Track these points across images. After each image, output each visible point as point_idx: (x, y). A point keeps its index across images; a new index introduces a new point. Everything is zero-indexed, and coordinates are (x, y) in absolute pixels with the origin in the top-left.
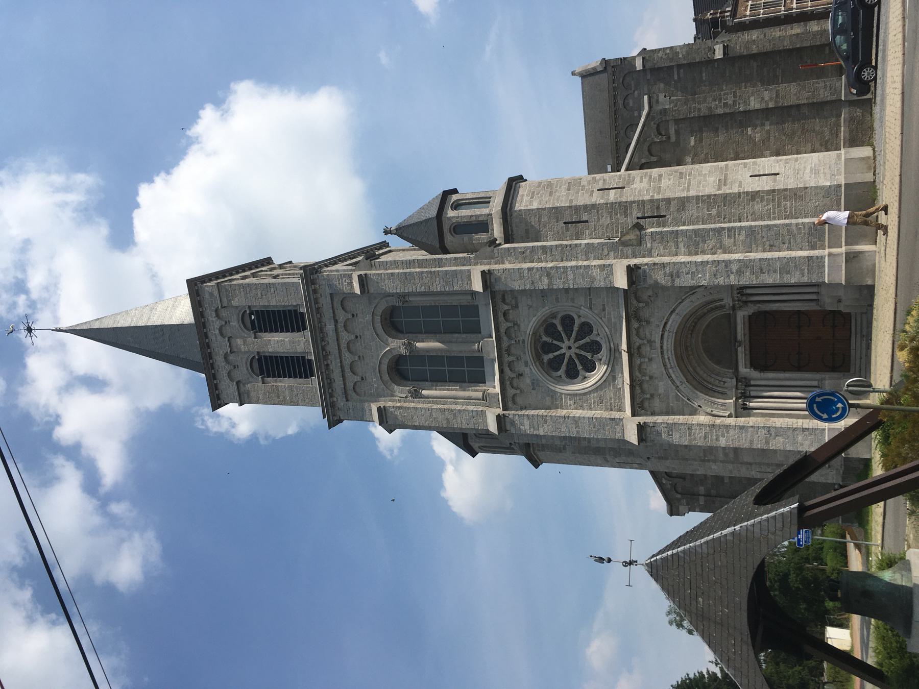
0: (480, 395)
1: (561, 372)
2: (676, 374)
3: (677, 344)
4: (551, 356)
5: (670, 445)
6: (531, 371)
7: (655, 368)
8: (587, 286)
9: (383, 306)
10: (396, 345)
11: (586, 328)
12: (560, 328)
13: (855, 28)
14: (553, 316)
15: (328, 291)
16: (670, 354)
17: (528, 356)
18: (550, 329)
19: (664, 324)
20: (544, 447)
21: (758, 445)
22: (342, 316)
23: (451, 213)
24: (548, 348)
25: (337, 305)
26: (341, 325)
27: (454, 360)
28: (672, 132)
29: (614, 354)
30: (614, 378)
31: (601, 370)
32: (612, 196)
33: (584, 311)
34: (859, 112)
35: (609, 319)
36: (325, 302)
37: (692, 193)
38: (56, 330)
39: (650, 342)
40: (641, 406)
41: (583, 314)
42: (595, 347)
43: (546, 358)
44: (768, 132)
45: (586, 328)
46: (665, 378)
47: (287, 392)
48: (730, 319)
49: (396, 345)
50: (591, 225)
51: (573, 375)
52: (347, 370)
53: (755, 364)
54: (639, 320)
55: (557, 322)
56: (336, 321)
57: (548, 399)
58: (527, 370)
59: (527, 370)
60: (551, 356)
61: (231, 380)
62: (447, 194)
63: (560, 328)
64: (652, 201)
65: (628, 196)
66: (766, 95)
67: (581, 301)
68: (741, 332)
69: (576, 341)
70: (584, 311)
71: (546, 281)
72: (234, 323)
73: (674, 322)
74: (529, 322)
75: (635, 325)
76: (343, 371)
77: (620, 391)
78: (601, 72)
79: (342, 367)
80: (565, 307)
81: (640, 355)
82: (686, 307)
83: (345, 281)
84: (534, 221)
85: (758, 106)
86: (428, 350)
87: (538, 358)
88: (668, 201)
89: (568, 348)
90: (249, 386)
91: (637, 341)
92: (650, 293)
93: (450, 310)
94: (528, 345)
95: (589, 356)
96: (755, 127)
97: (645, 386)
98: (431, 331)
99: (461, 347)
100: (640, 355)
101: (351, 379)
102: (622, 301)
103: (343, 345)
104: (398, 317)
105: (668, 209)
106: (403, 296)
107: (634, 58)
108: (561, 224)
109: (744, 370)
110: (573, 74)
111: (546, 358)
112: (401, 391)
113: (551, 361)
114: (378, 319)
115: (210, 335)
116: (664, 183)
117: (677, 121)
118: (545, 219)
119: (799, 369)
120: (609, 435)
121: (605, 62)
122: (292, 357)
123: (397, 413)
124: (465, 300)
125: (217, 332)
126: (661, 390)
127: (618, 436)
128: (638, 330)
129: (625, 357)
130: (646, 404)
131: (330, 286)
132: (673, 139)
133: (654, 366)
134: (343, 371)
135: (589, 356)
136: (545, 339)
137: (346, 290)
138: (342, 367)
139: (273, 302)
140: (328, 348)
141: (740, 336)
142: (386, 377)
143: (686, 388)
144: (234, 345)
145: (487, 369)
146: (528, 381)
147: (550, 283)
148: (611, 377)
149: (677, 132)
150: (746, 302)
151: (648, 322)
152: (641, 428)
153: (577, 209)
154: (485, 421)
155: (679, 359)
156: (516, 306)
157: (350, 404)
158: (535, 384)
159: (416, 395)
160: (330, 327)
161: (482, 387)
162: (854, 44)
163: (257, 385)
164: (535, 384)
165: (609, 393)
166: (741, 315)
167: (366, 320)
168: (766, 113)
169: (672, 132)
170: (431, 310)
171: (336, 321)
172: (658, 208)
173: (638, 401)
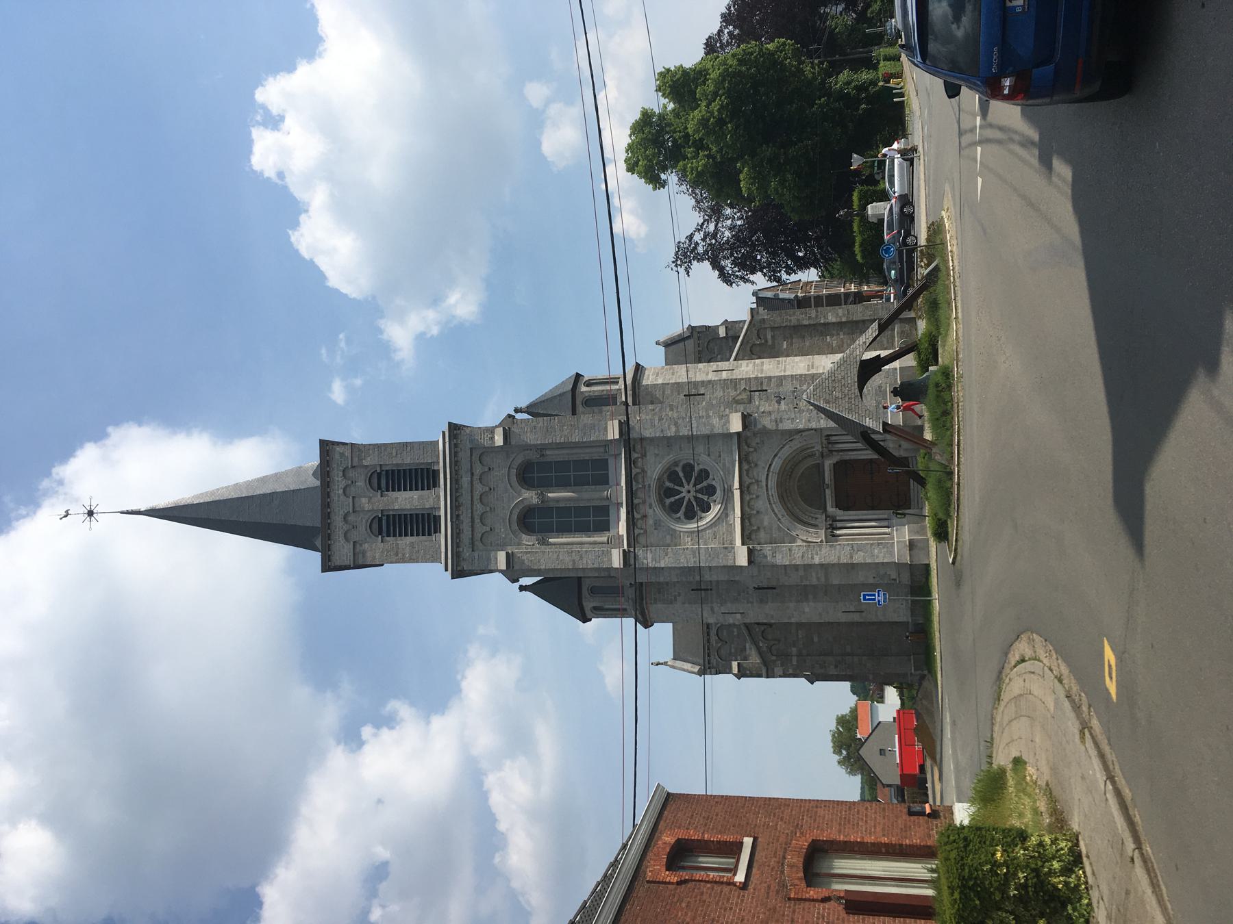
0: (605, 539)
1: (681, 514)
2: (778, 508)
3: (780, 485)
4: (672, 499)
5: (774, 566)
6: (654, 512)
7: (761, 504)
8: (708, 432)
9: (520, 459)
10: (530, 496)
11: (704, 474)
12: (681, 474)
13: (901, 261)
14: (676, 464)
15: (469, 446)
16: (773, 491)
17: (653, 499)
18: (672, 476)
19: (770, 462)
20: (661, 588)
21: (844, 560)
22: (478, 470)
23: (584, 389)
24: (669, 492)
25: (475, 458)
26: (475, 477)
27: (581, 511)
28: (769, 337)
29: (728, 493)
30: (727, 515)
31: (715, 509)
32: (724, 375)
33: (704, 458)
34: (907, 327)
35: (724, 464)
36: (464, 456)
37: (787, 373)
38: (128, 512)
39: (757, 481)
40: (749, 538)
41: (703, 460)
42: (711, 490)
43: (668, 501)
44: (842, 340)
45: (704, 474)
46: (771, 514)
47: (407, 550)
48: (819, 468)
49: (530, 496)
50: (707, 397)
51: (690, 515)
52: (477, 520)
53: (839, 505)
54: (749, 463)
55: (679, 469)
56: (472, 474)
57: (668, 537)
58: (650, 512)
59: (650, 512)
60: (672, 499)
61: (347, 539)
62: (578, 376)
63: (681, 474)
64: (756, 378)
65: (737, 375)
66: (840, 311)
67: (700, 449)
68: (828, 476)
69: (695, 485)
70: (704, 458)
71: (673, 429)
72: (360, 484)
73: (777, 464)
74: (655, 468)
75: (746, 467)
76: (473, 522)
77: (732, 526)
78: (688, 337)
79: (472, 518)
80: (685, 455)
81: (749, 493)
82: (786, 452)
83: (487, 436)
84: (658, 394)
85: (834, 320)
86: (557, 500)
87: (661, 502)
88: (770, 378)
89: (687, 492)
90: (366, 546)
91: (747, 481)
92: (758, 440)
93: (581, 464)
94: (653, 489)
95: (705, 498)
96: (832, 336)
97: (753, 520)
98: (563, 484)
99: (590, 495)
100: (749, 493)
101: (480, 529)
102: (735, 447)
103: (476, 497)
104: (533, 471)
105: (769, 384)
106: (541, 449)
107: (717, 327)
108: (682, 396)
109: (831, 510)
110: (657, 343)
111: (668, 501)
112: (528, 540)
113: (672, 504)
114: (514, 471)
115: (332, 494)
116: (765, 367)
117: (773, 329)
118: (668, 392)
119: (873, 509)
120: (722, 563)
121: (692, 329)
122: (417, 515)
123: (525, 557)
124: (596, 454)
125: (341, 491)
126: (766, 523)
127: (730, 563)
128: (747, 471)
129: (737, 494)
130: (753, 537)
131: (472, 441)
132: (770, 342)
133: (761, 502)
134: (473, 522)
135: (705, 498)
136: (668, 484)
137: (487, 443)
138: (472, 518)
139: (408, 461)
140: (461, 500)
141: (827, 480)
142: (515, 526)
143: (786, 520)
144: (357, 505)
145: (612, 518)
146: (651, 522)
147: (677, 431)
148: (725, 514)
149: (773, 337)
150: (831, 451)
151: (756, 465)
152: (750, 552)
153: (696, 384)
154: (610, 560)
155: (781, 497)
156: (644, 456)
157: (476, 554)
158: (657, 524)
159: (543, 542)
160: (465, 480)
161: (607, 534)
162: (900, 272)
163: (375, 547)
164: (657, 524)
165: (722, 528)
166: (828, 463)
167: (502, 475)
168: (840, 325)
169: (769, 337)
170: (563, 465)
171: (472, 474)
172: (762, 384)
173: (747, 532)
